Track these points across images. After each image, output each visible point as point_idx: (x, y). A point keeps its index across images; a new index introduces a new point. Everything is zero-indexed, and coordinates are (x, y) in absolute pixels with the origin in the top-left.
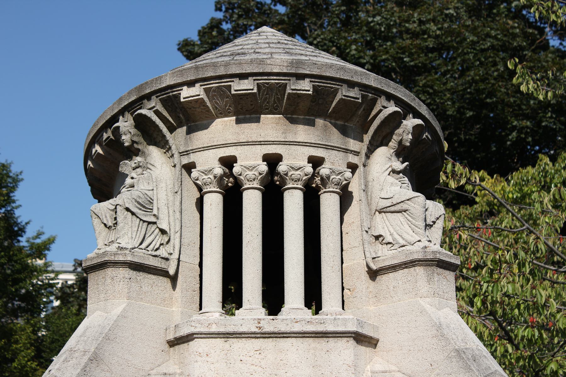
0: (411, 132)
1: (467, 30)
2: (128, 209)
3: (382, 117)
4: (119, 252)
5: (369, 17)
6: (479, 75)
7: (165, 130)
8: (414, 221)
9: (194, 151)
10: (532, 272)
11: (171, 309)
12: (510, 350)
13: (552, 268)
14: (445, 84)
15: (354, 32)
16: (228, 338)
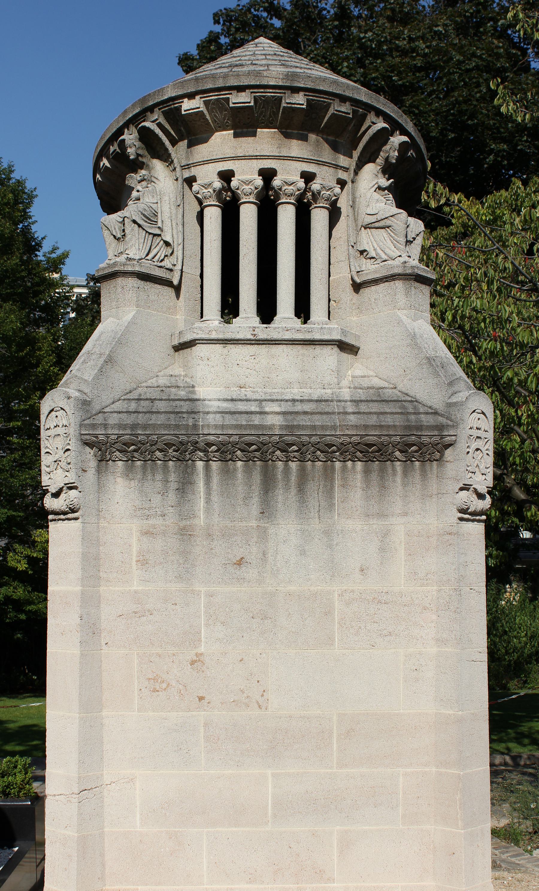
0: (397, 149)
1: (454, 49)
2: (134, 222)
3: (371, 132)
4: (128, 263)
5: (361, 32)
6: (463, 96)
7: (167, 143)
8: (396, 237)
9: (195, 165)
10: (499, 290)
11: (176, 316)
12: (474, 361)
13: (516, 286)
14: (430, 104)
15: (346, 49)
16: (226, 344)
